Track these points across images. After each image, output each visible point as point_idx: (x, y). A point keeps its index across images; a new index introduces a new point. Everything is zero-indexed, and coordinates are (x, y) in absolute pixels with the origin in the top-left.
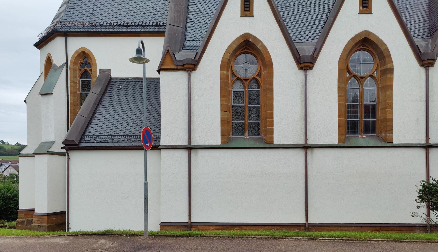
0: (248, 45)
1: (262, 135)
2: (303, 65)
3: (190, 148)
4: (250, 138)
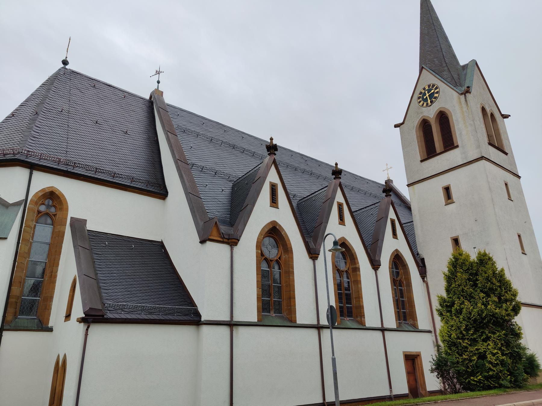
0: (274, 232)
1: (285, 314)
2: (314, 255)
3: (231, 325)
4: (276, 316)
